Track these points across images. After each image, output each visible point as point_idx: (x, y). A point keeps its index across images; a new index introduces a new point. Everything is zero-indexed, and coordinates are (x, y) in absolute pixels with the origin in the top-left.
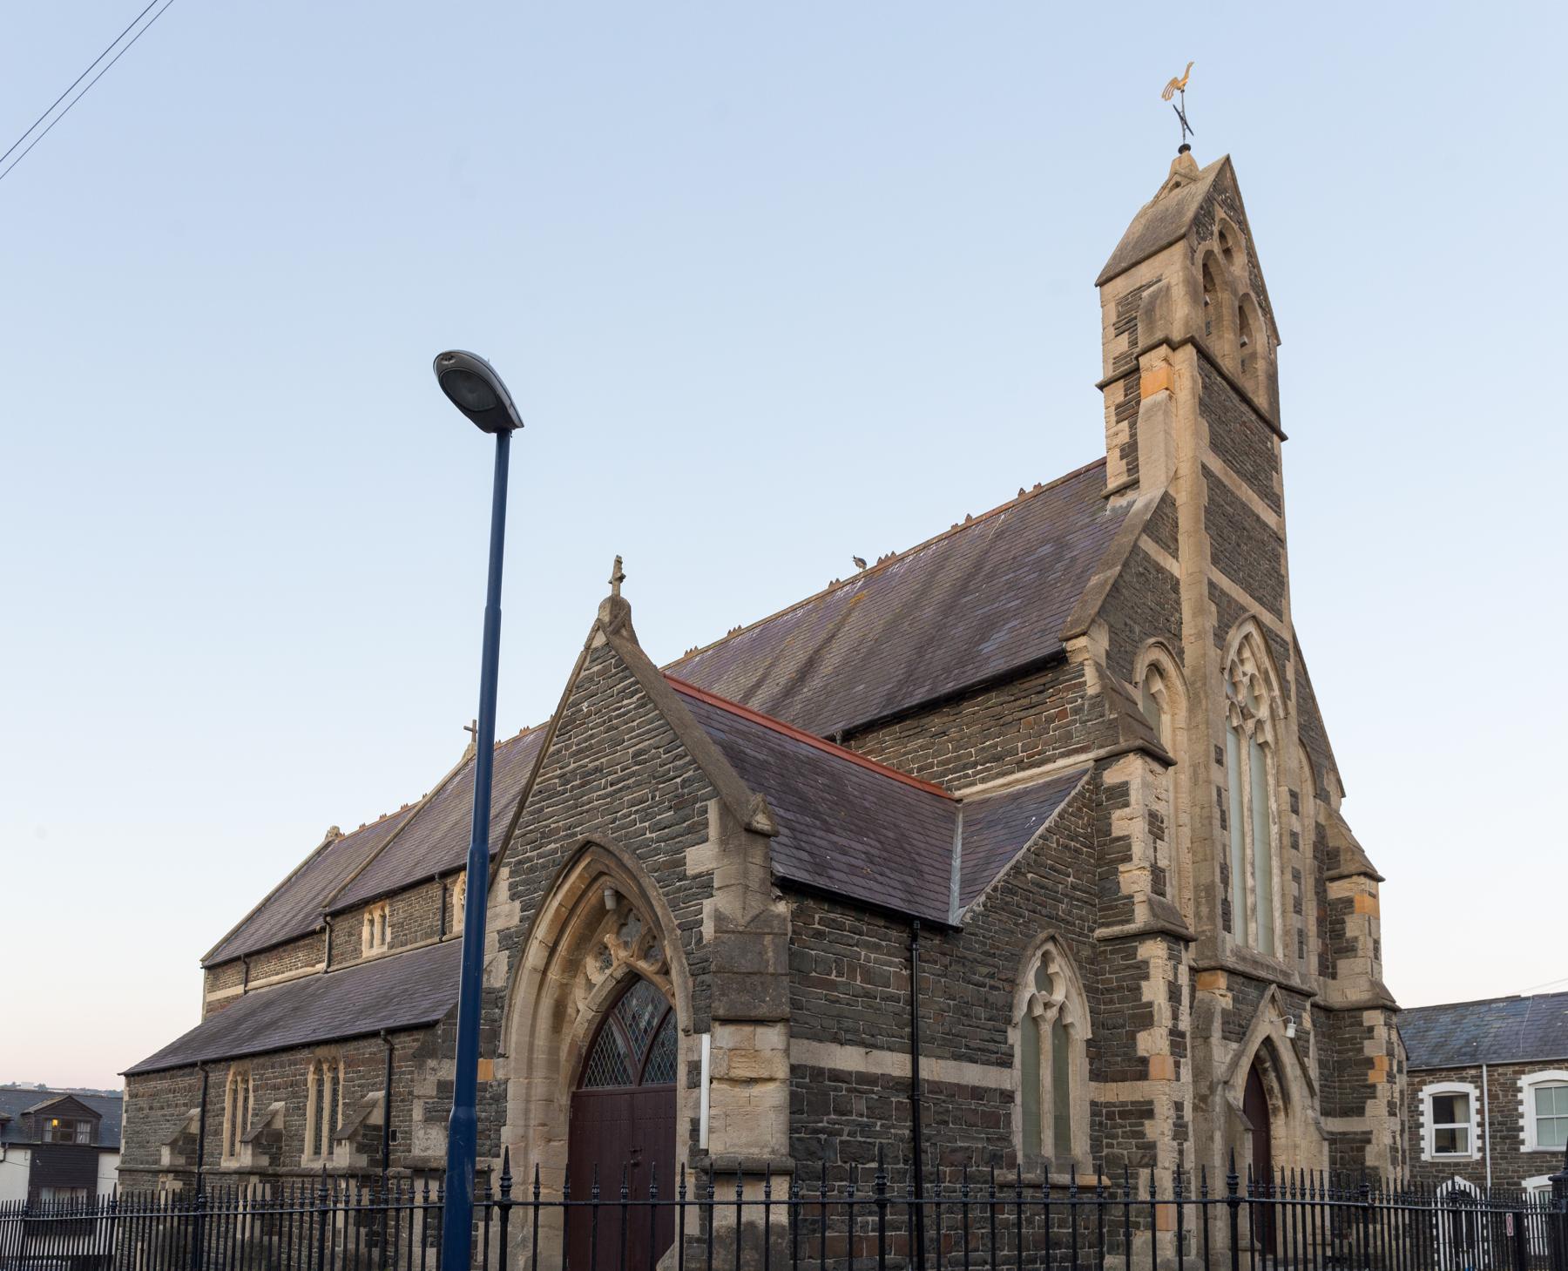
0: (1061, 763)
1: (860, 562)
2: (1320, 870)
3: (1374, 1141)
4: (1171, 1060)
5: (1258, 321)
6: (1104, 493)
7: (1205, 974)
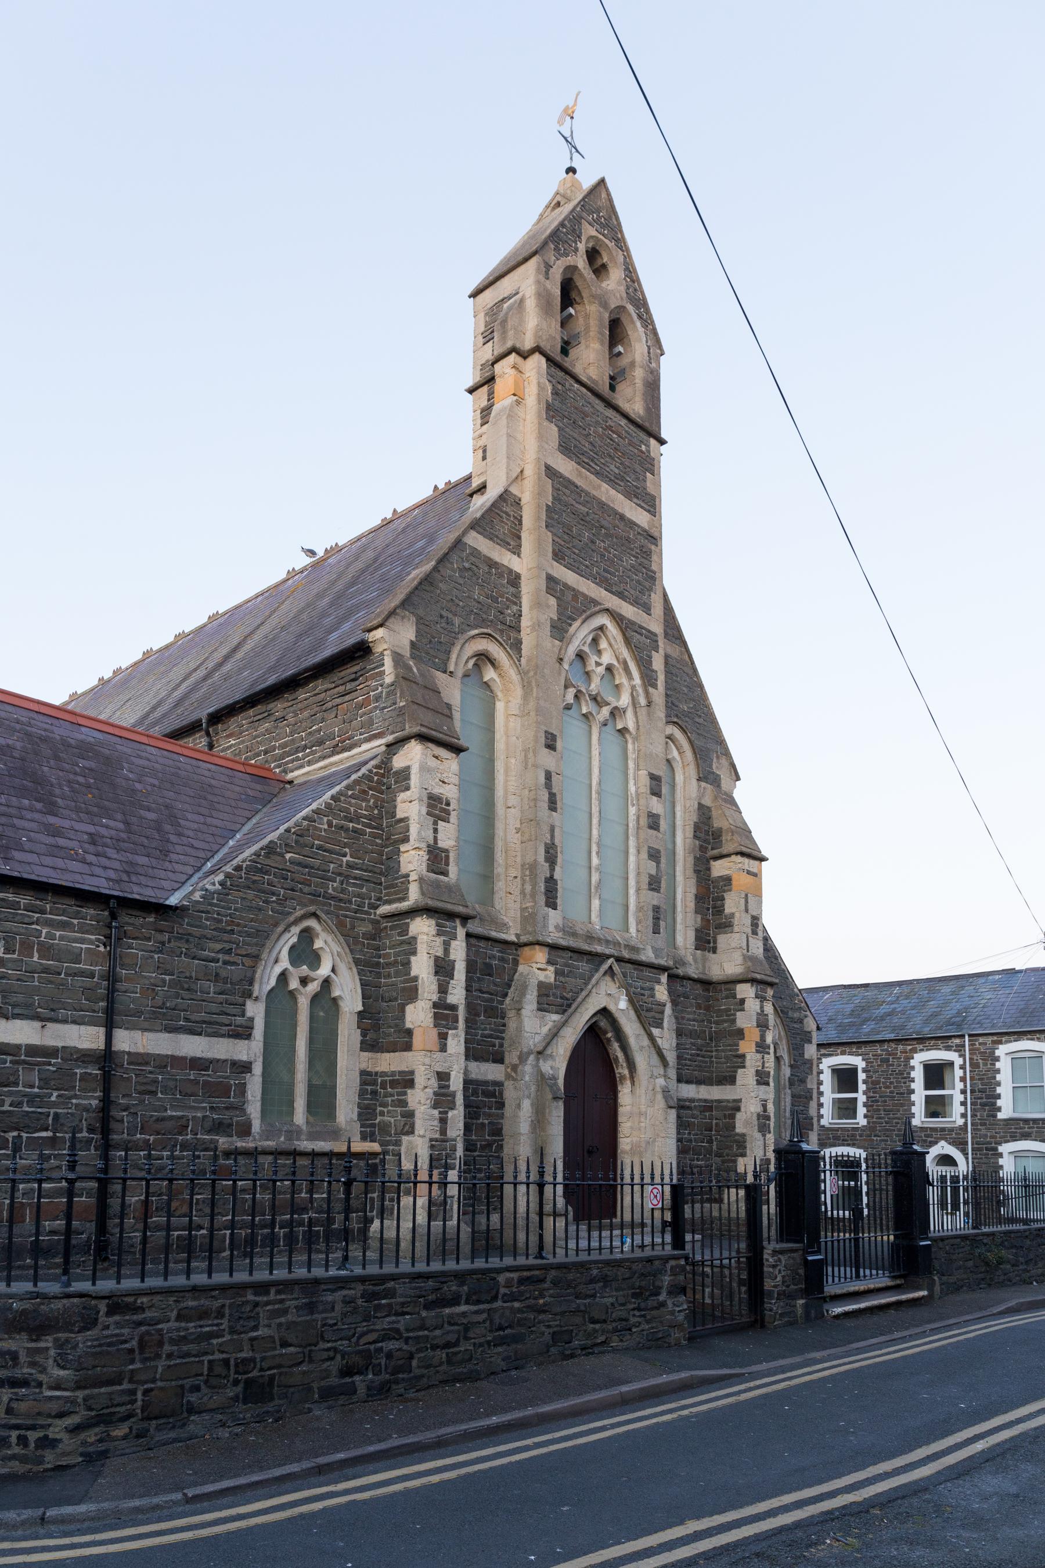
0: (365, 746)
1: (311, 553)
2: (702, 849)
3: (743, 1109)
4: (434, 1033)
5: (636, 332)
6: (468, 491)
7: (526, 949)
